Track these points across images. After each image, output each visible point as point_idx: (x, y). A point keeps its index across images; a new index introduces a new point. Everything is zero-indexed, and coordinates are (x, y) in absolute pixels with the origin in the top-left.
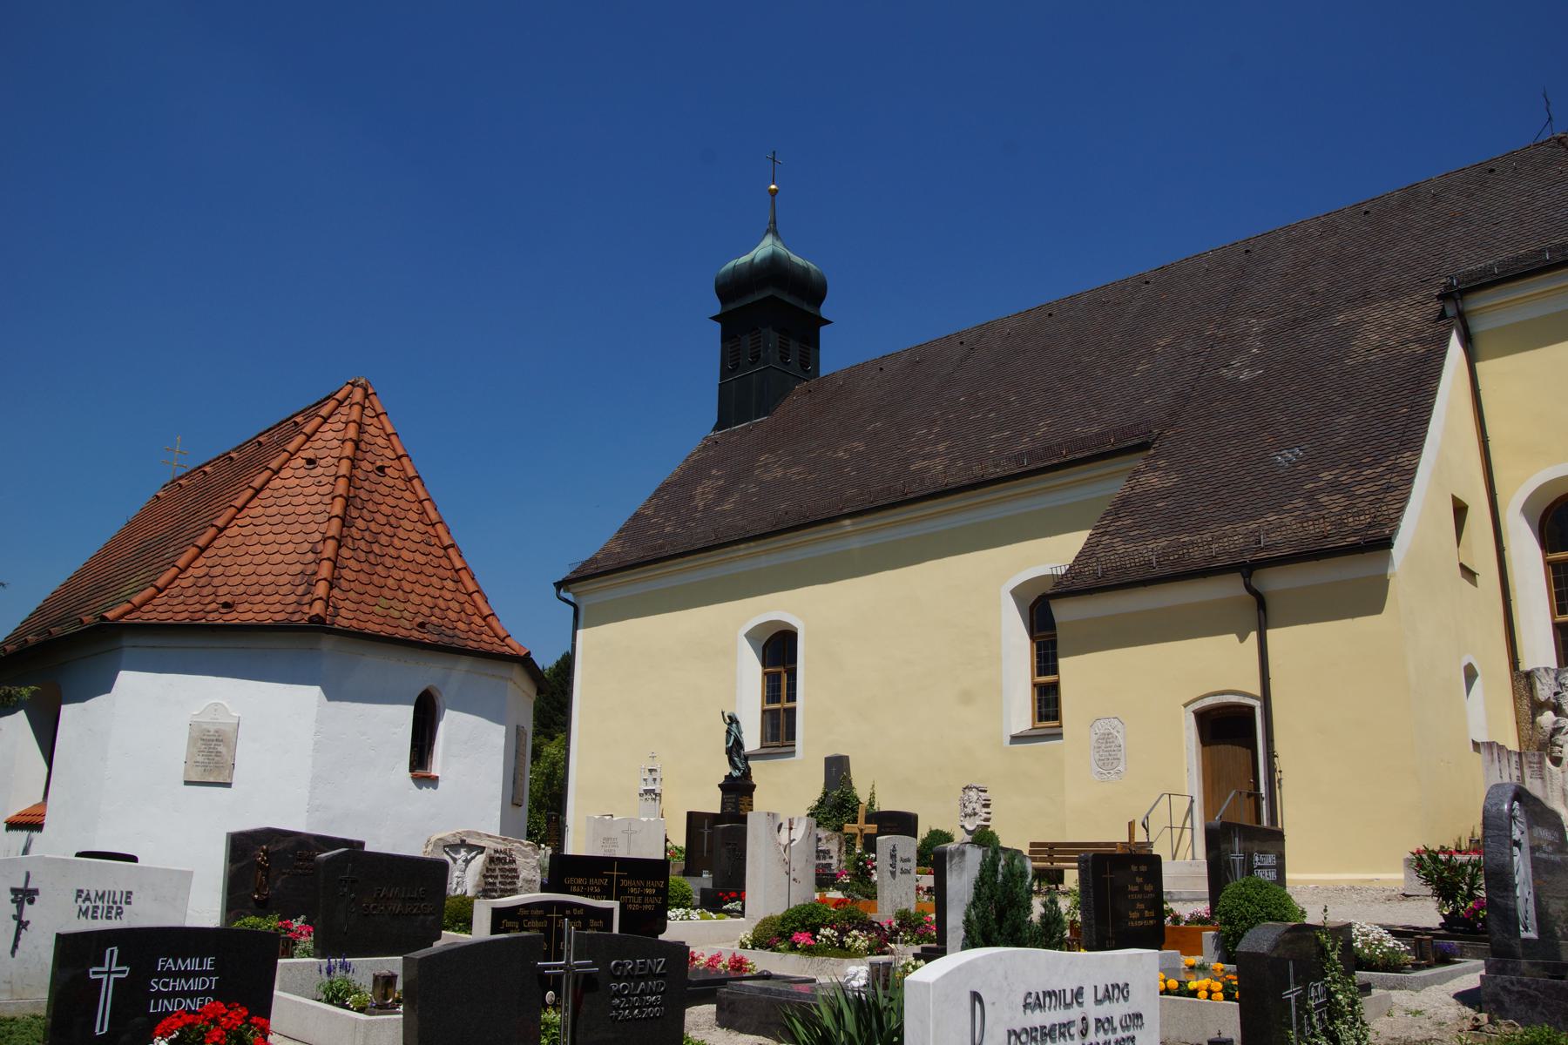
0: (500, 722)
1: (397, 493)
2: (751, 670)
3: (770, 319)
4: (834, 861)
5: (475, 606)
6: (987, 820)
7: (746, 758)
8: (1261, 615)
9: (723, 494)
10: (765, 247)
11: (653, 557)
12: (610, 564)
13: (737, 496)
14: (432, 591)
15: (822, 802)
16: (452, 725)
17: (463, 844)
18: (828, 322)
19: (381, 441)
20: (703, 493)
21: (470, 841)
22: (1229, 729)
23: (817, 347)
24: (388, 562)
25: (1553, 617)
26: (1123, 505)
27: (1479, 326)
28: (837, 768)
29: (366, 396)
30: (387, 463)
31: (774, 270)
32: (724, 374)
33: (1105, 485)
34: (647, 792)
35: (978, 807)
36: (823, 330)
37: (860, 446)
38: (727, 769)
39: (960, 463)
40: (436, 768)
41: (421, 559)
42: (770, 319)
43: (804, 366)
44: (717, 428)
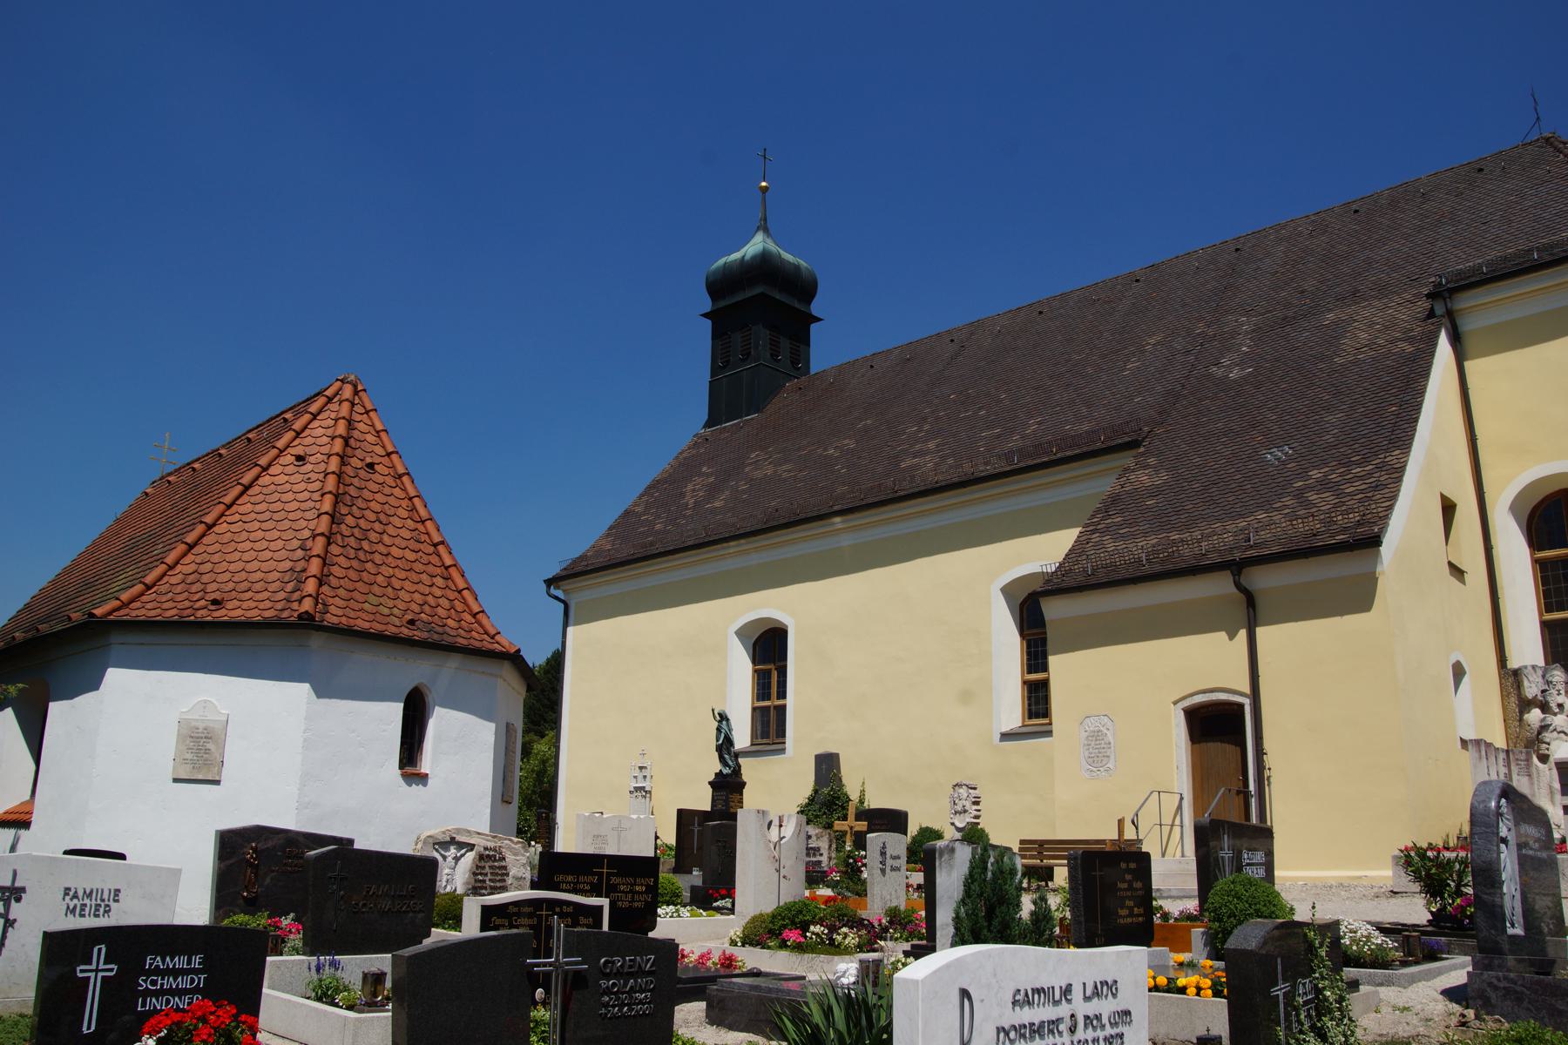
0: (490, 719)
1: (387, 490)
2: (741, 667)
3: (760, 315)
4: (824, 859)
5: (465, 603)
7: (737, 755)
8: (1251, 613)
9: (713, 491)
10: (756, 245)
11: (643, 555)
12: (601, 561)
14: (421, 588)
15: (812, 800)
16: (442, 722)
17: (453, 841)
18: (819, 320)
19: (370, 438)
20: (693, 490)
21: (460, 838)
22: (1218, 727)
24: (378, 558)
25: (1541, 615)
26: (1112, 503)
27: (1468, 325)
28: (827, 765)
29: (356, 392)
30: (377, 459)
31: (764, 267)
32: (715, 370)
33: (1096, 483)
34: (637, 789)
35: (968, 805)
36: (814, 327)
38: (717, 766)
40: (426, 766)
41: (411, 556)
42: (760, 315)
43: (794, 363)
44: (708, 425)
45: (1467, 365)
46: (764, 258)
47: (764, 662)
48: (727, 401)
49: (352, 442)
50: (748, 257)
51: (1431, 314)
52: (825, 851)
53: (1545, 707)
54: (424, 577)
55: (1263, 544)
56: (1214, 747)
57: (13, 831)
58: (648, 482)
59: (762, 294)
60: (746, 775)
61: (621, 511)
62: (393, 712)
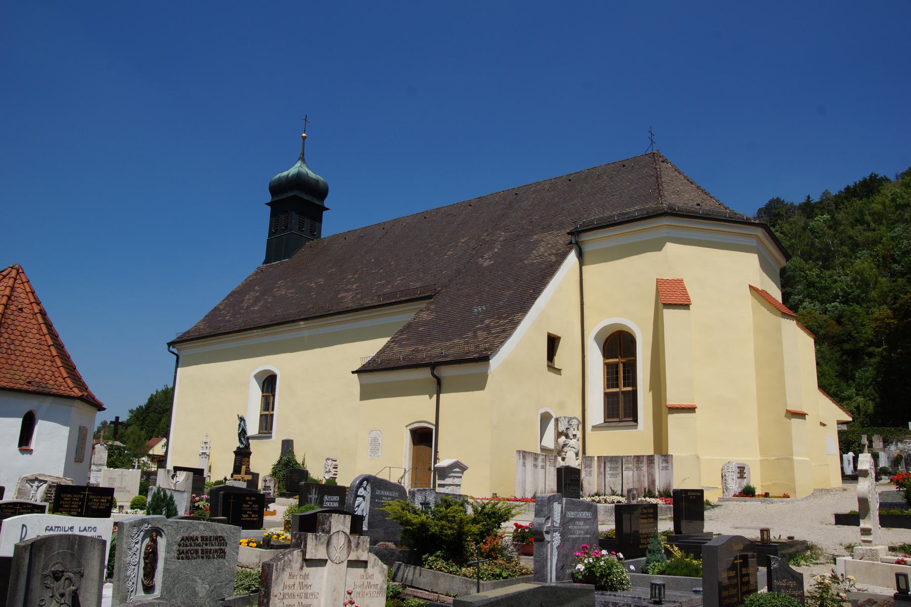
0: (66, 425)
1: (28, 321)
2: (256, 393)
3: (296, 206)
4: (272, 492)
5: (60, 373)
7: (248, 439)
8: (439, 387)
9: (257, 300)
10: (293, 171)
11: (218, 333)
12: (196, 335)
14: (38, 366)
15: (279, 462)
16: (41, 427)
17: (36, 479)
19: (23, 296)
20: (249, 298)
21: (40, 478)
22: (423, 437)
24: (18, 353)
27: (587, 249)
28: (287, 446)
29: (18, 273)
30: (24, 306)
31: (299, 181)
32: (271, 234)
33: (403, 316)
34: (203, 453)
35: (331, 468)
36: (325, 213)
38: (238, 444)
39: (359, 296)
40: (33, 445)
41: (35, 351)
42: (296, 206)
44: (265, 262)
46: (299, 177)
47: (267, 392)
48: (277, 249)
49: (13, 298)
51: (571, 243)
52: (272, 488)
53: (567, 436)
54: (41, 361)
55: (446, 356)
56: (423, 448)
58: (229, 292)
60: (252, 448)
61: (213, 307)
62: (18, 422)
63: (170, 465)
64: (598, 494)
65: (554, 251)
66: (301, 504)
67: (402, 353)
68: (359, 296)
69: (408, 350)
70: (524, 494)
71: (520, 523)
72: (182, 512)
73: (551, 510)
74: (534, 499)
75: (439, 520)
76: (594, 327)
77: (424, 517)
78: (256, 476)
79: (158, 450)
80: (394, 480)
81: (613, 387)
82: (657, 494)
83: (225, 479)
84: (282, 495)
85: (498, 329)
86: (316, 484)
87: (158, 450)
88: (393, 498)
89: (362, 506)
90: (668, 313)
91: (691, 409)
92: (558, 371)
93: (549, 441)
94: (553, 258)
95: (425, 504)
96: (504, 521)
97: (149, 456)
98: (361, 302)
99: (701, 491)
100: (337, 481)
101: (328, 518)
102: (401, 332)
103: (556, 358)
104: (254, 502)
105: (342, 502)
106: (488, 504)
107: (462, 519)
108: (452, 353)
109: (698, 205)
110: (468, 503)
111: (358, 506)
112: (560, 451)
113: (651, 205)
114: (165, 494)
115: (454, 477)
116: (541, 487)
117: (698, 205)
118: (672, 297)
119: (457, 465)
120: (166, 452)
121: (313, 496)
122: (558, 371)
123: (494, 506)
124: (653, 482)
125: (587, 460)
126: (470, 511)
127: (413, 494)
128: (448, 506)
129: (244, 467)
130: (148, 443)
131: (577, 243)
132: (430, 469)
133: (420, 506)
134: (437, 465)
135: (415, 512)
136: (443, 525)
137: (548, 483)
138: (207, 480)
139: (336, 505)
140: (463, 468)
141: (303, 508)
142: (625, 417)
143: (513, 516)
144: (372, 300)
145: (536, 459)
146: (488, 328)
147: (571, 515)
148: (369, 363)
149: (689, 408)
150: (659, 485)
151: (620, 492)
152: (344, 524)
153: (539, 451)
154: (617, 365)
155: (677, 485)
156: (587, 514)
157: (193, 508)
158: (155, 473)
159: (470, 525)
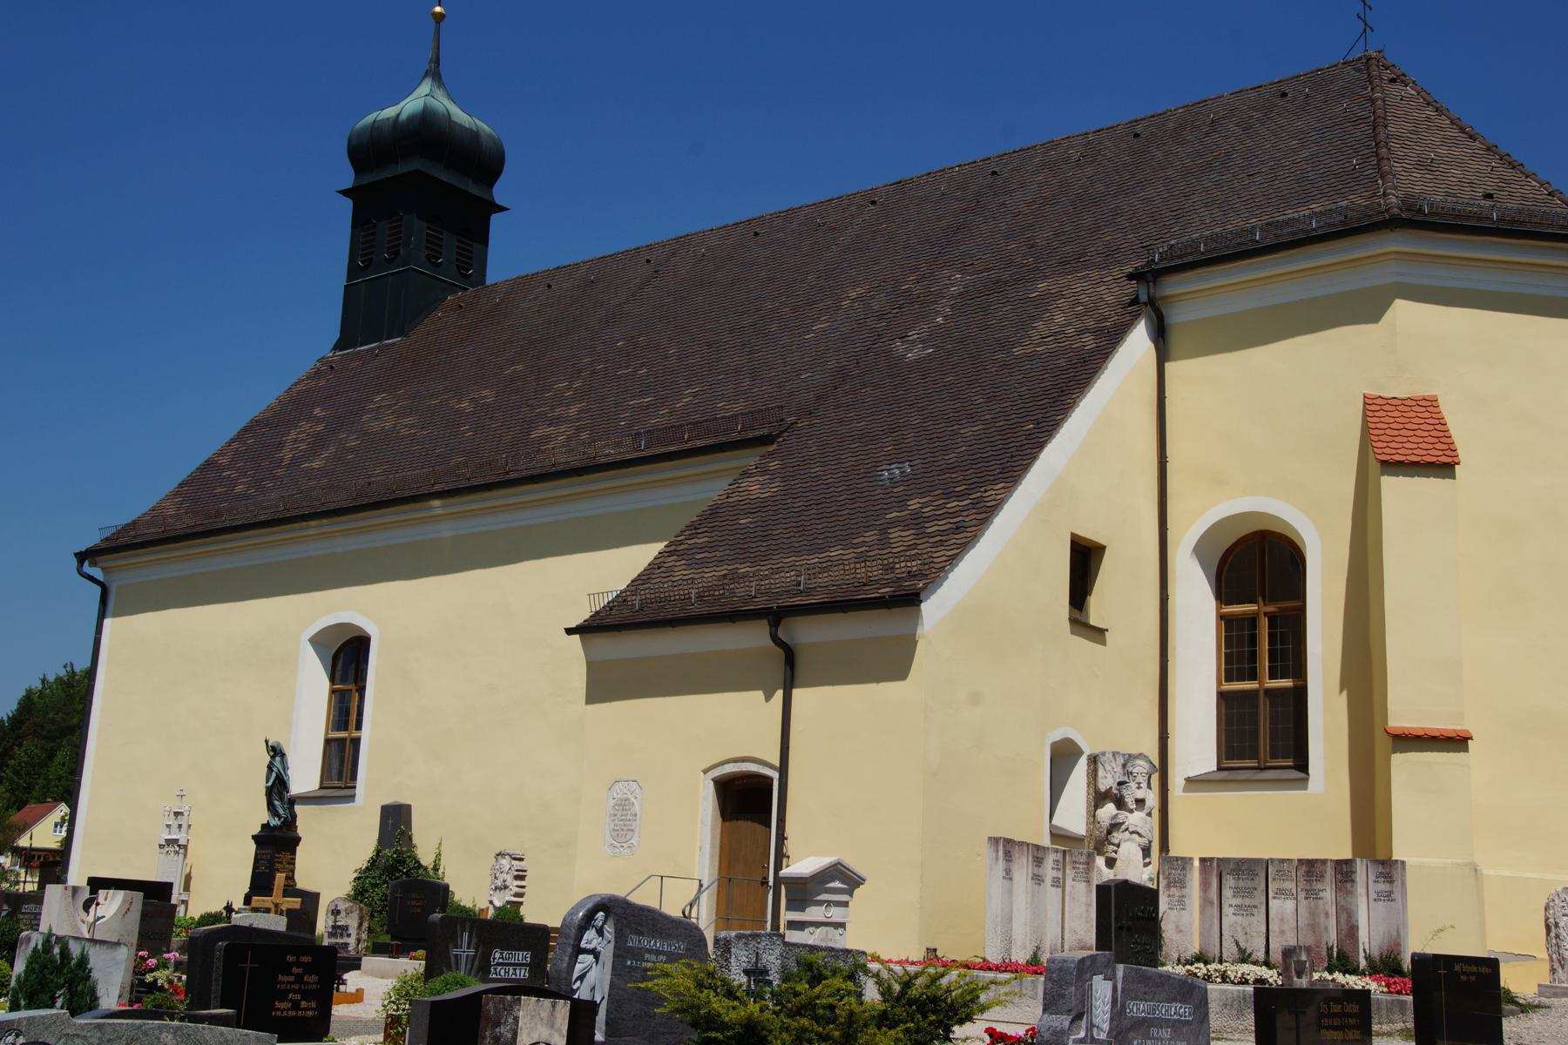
2: (314, 685)
3: (420, 202)
4: (352, 941)
6: (521, 895)
7: (292, 802)
8: (789, 672)
9: (318, 443)
10: (410, 105)
11: (208, 531)
12: (153, 531)
13: (332, 449)
15: (373, 863)
18: (503, 209)
20: (296, 438)
22: (747, 800)
23: (485, 242)
25: (1219, 683)
26: (712, 516)
27: (1178, 316)
28: (396, 819)
31: (426, 134)
32: (353, 271)
33: (699, 488)
34: (170, 842)
35: (509, 878)
36: (495, 219)
37: (488, 395)
39: (584, 436)
42: (420, 202)
43: (462, 269)
45: (1170, 367)
47: (343, 681)
48: (372, 311)
50: (403, 117)
51: (1135, 301)
52: (353, 931)
53: (1120, 803)
55: (809, 591)
56: (746, 827)
57: (777, 764)
59: (417, 172)
60: (302, 828)
61: (200, 461)
63: (77, 874)
64: (1201, 958)
65: (1091, 323)
66: (430, 973)
67: (697, 581)
68: (584, 436)
69: (711, 575)
70: (1008, 951)
71: (1000, 1028)
72: (111, 995)
73: (1085, 997)
74: (1034, 966)
75: (792, 1015)
76: (1194, 521)
77: (753, 1007)
78: (311, 899)
79: (44, 835)
80: (673, 909)
81: (1241, 678)
82: (1363, 963)
83: (229, 909)
84: (378, 949)
85: (944, 525)
86: (470, 920)
87: (44, 835)
88: (672, 958)
89: (591, 977)
90: (1394, 489)
91: (1457, 742)
92: (1098, 634)
93: (1073, 814)
94: (1089, 342)
95: (757, 973)
96: (961, 1022)
97: (18, 852)
98: (592, 452)
99: (1492, 964)
100: (523, 910)
101: (509, 1008)
102: (693, 528)
103: (1093, 601)
104: (308, 969)
105: (537, 966)
106: (917, 976)
107: (852, 1013)
108: (827, 584)
109: (1489, 196)
110: (866, 971)
111: (581, 978)
112: (1102, 842)
113: (1355, 200)
114: (65, 953)
115: (829, 903)
116: (1051, 936)
117: (1489, 196)
118: (1406, 443)
119: (837, 872)
120: (68, 842)
121: (464, 950)
122: (1098, 634)
123: (934, 980)
124: (1352, 931)
125: (1174, 867)
126: (871, 994)
127: (724, 946)
128: (816, 979)
129: (280, 877)
130: (15, 817)
131: (1152, 302)
132: (765, 882)
133: (744, 979)
134: (784, 872)
135: (730, 994)
136: (804, 1030)
137: (1072, 924)
138: (181, 910)
139: (523, 973)
140: (853, 882)
141: (436, 983)
142: (1274, 756)
143: (983, 1009)
144: (618, 445)
145: (1038, 861)
146: (917, 522)
147: (1138, 1009)
148: (610, 607)
149: (1450, 739)
150: (1369, 940)
151: (1261, 955)
152: (551, 1024)
153: (1046, 841)
154: (1252, 620)
155: (1420, 941)
156: (1179, 1010)
157: (140, 988)
158: (37, 898)
159: (871, 1031)
